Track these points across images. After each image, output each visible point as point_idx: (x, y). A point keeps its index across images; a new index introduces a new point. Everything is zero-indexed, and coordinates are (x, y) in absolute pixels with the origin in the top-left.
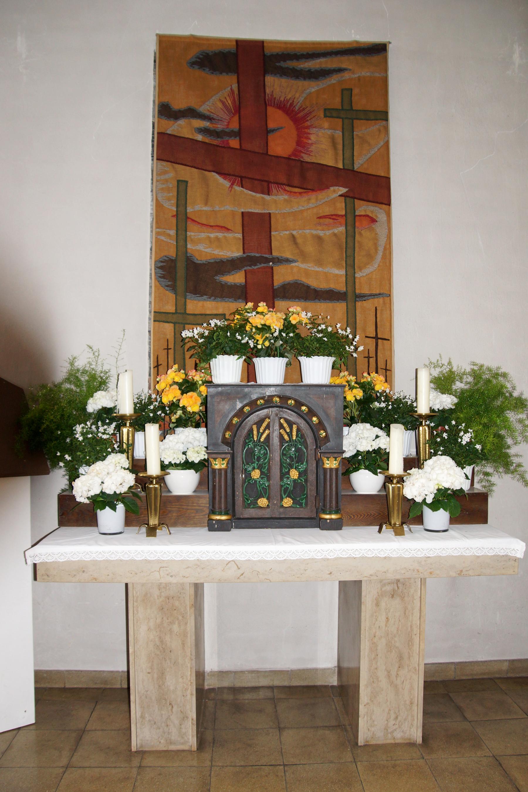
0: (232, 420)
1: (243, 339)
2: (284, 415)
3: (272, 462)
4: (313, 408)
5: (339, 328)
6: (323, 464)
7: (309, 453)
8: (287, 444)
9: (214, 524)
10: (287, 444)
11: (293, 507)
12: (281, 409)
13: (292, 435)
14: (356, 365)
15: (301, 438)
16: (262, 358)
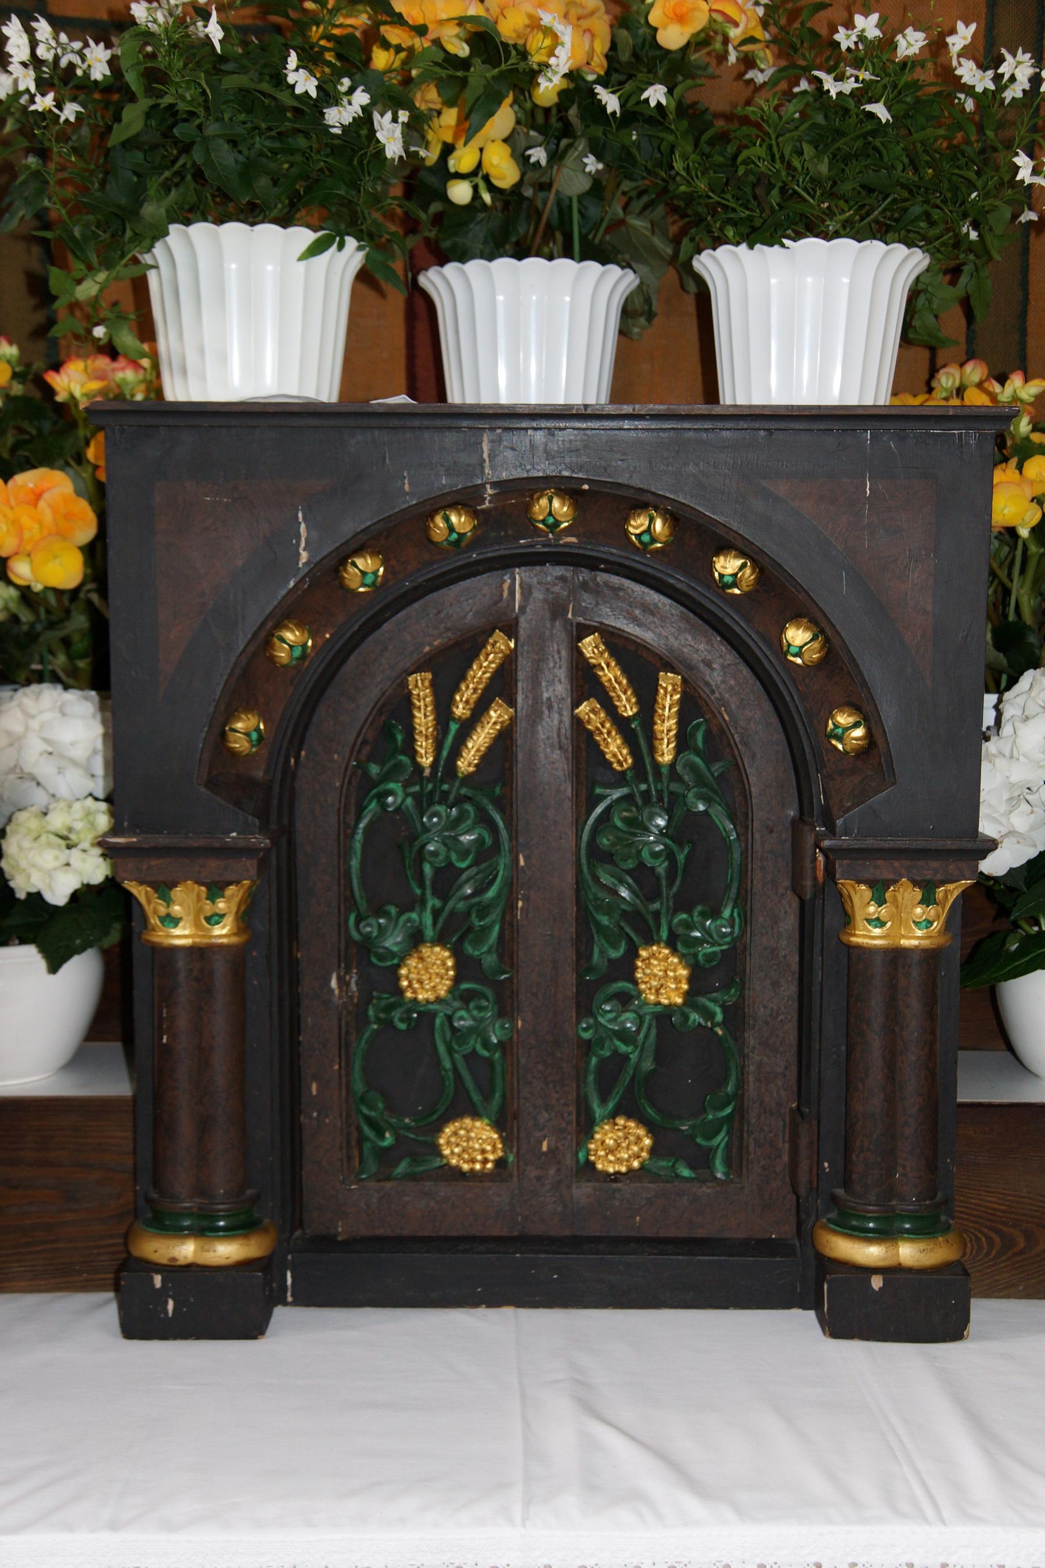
0: (267, 644)
1: (328, 96)
2: (606, 610)
3: (526, 899)
4: (790, 565)
5: (964, 53)
6: (847, 920)
7: (757, 846)
8: (617, 794)
9: (161, 1296)
10: (617, 794)
11: (656, 1178)
12: (584, 575)
13: (651, 737)
14: (1023, 332)
15: (711, 755)
16: (475, 267)
